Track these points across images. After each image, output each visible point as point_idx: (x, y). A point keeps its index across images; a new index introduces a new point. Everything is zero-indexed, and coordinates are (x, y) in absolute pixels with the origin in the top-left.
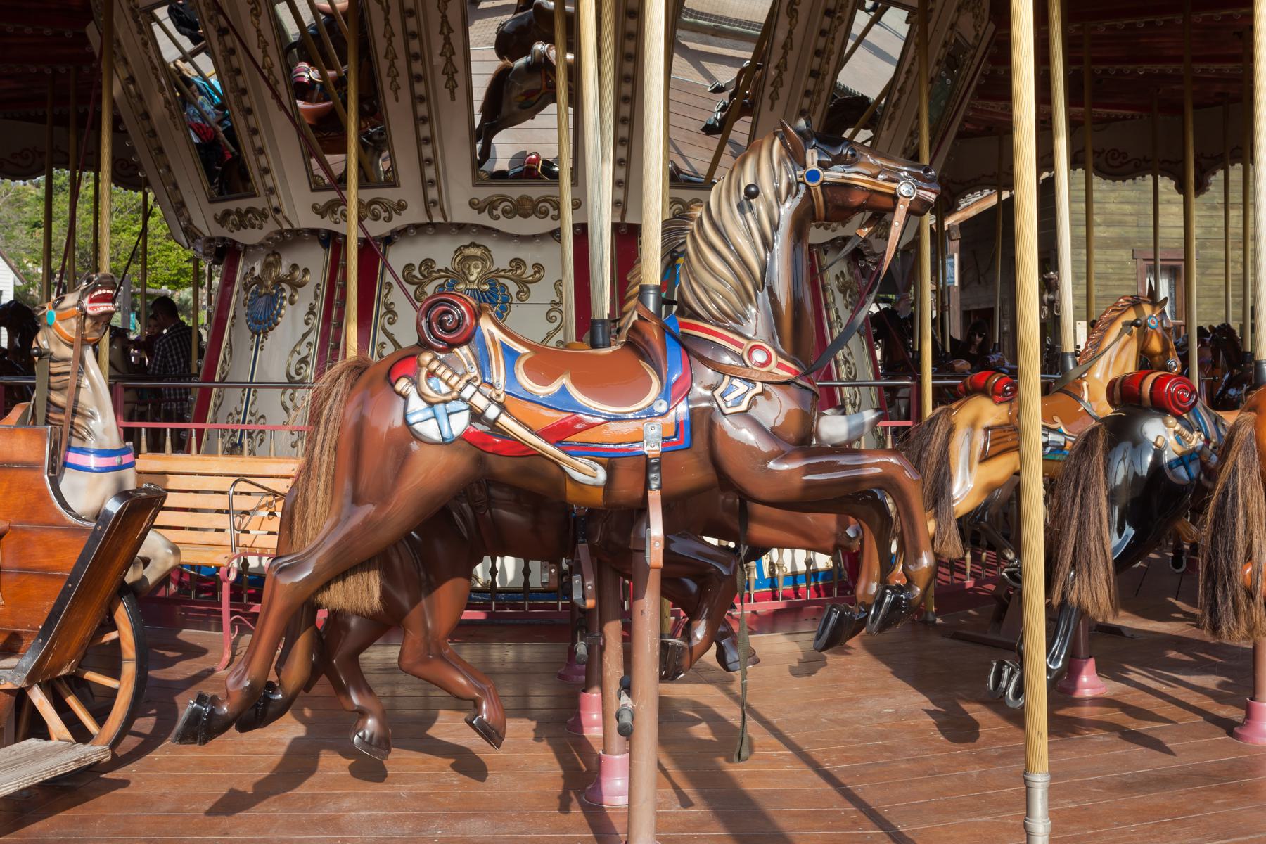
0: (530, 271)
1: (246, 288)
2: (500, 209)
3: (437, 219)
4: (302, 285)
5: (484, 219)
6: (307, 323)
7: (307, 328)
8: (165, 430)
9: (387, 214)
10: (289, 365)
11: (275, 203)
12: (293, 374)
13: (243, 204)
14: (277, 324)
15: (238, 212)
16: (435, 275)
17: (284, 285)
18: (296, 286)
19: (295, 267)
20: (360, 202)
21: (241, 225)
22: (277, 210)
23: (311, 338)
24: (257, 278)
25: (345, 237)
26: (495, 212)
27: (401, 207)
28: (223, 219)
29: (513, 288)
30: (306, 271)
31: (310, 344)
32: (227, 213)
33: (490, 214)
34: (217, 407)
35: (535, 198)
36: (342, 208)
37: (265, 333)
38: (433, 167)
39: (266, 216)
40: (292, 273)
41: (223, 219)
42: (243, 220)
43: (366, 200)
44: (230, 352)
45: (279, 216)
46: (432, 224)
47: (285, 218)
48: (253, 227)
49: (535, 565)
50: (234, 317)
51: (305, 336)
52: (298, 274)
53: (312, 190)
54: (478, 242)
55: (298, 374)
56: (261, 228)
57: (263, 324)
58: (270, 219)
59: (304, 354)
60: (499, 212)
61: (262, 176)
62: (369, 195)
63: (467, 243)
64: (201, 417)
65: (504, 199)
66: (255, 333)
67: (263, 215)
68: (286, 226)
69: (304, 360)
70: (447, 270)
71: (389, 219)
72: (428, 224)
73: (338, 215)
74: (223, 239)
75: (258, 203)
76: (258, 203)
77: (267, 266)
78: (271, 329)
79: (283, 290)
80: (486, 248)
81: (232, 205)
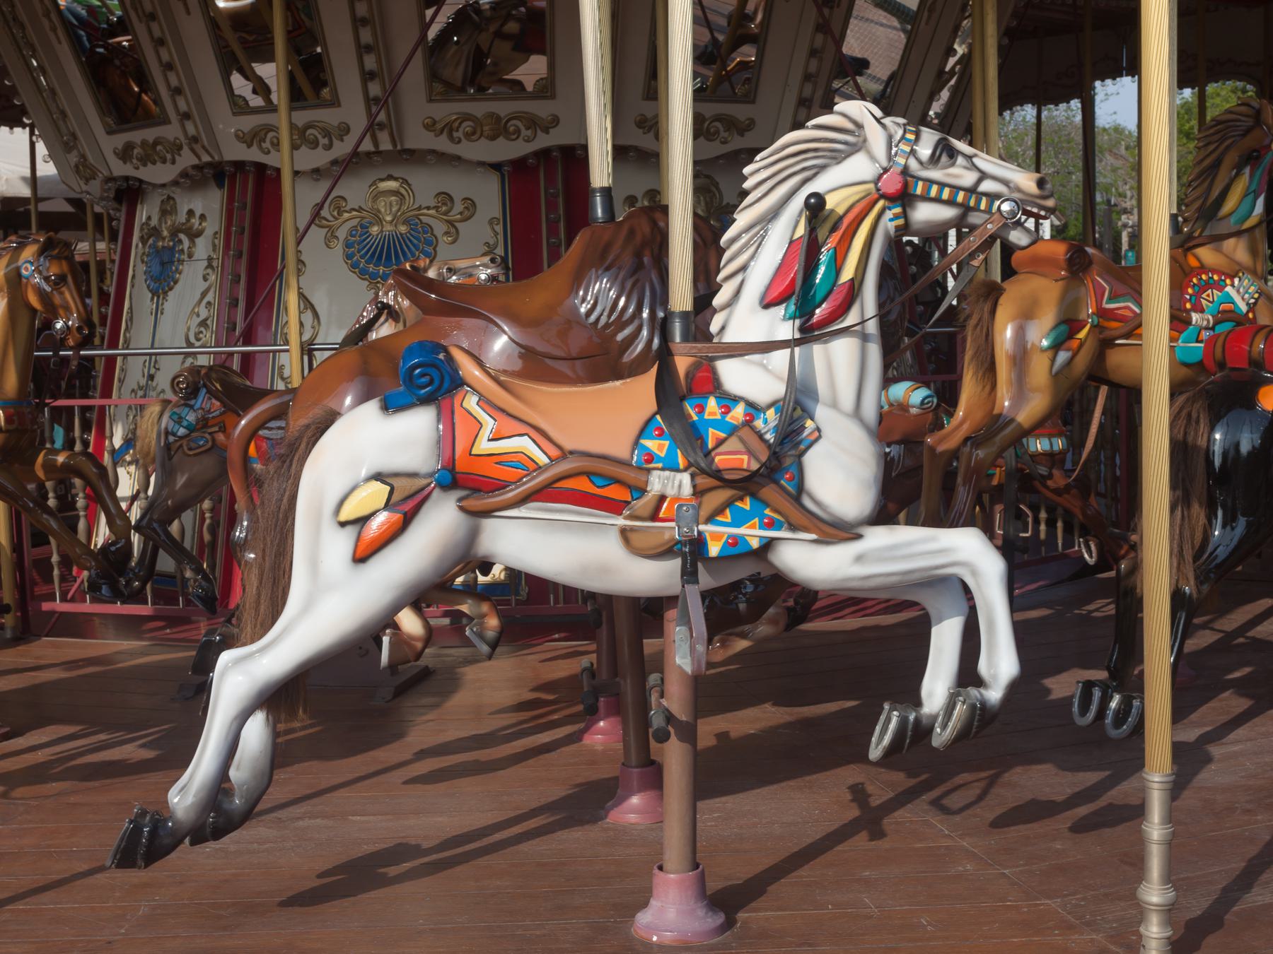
0: (459, 207)
1: (143, 240)
2: (268, 140)
3: (386, 145)
4: (199, 234)
5: (442, 144)
6: (205, 279)
7: (207, 284)
8: (72, 408)
9: (326, 141)
10: (189, 329)
11: (191, 130)
12: (192, 339)
13: (150, 134)
14: (176, 282)
15: (144, 143)
16: (346, 215)
17: (182, 236)
18: (194, 235)
19: (191, 213)
20: (292, 126)
21: (145, 160)
22: (195, 139)
23: (210, 297)
24: (154, 228)
25: (278, 171)
26: (455, 134)
27: (345, 130)
28: (125, 154)
29: (439, 228)
30: (203, 217)
31: (209, 303)
32: (129, 147)
33: (260, 148)
34: (121, 381)
35: (479, 116)
36: (271, 135)
37: (165, 293)
38: (377, 81)
39: (180, 148)
40: (188, 220)
41: (125, 154)
42: (150, 154)
43: (300, 124)
44: (131, 319)
45: (197, 147)
46: (378, 153)
47: (204, 147)
48: (164, 162)
49: (1054, 440)
50: (134, 276)
51: (204, 294)
52: (195, 221)
53: (234, 114)
54: (396, 175)
55: (198, 340)
56: (173, 162)
57: (162, 283)
58: (186, 151)
59: (203, 317)
60: (459, 134)
61: (173, 97)
62: (301, 117)
63: (384, 176)
64: (107, 393)
65: (466, 117)
66: (155, 293)
67: (177, 148)
68: (206, 158)
69: (203, 323)
70: (360, 209)
71: (329, 147)
72: (374, 153)
73: (267, 145)
74: (127, 179)
75: (171, 132)
76: (171, 132)
77: (164, 213)
78: (171, 289)
79: (180, 241)
80: (405, 181)
81: (137, 136)
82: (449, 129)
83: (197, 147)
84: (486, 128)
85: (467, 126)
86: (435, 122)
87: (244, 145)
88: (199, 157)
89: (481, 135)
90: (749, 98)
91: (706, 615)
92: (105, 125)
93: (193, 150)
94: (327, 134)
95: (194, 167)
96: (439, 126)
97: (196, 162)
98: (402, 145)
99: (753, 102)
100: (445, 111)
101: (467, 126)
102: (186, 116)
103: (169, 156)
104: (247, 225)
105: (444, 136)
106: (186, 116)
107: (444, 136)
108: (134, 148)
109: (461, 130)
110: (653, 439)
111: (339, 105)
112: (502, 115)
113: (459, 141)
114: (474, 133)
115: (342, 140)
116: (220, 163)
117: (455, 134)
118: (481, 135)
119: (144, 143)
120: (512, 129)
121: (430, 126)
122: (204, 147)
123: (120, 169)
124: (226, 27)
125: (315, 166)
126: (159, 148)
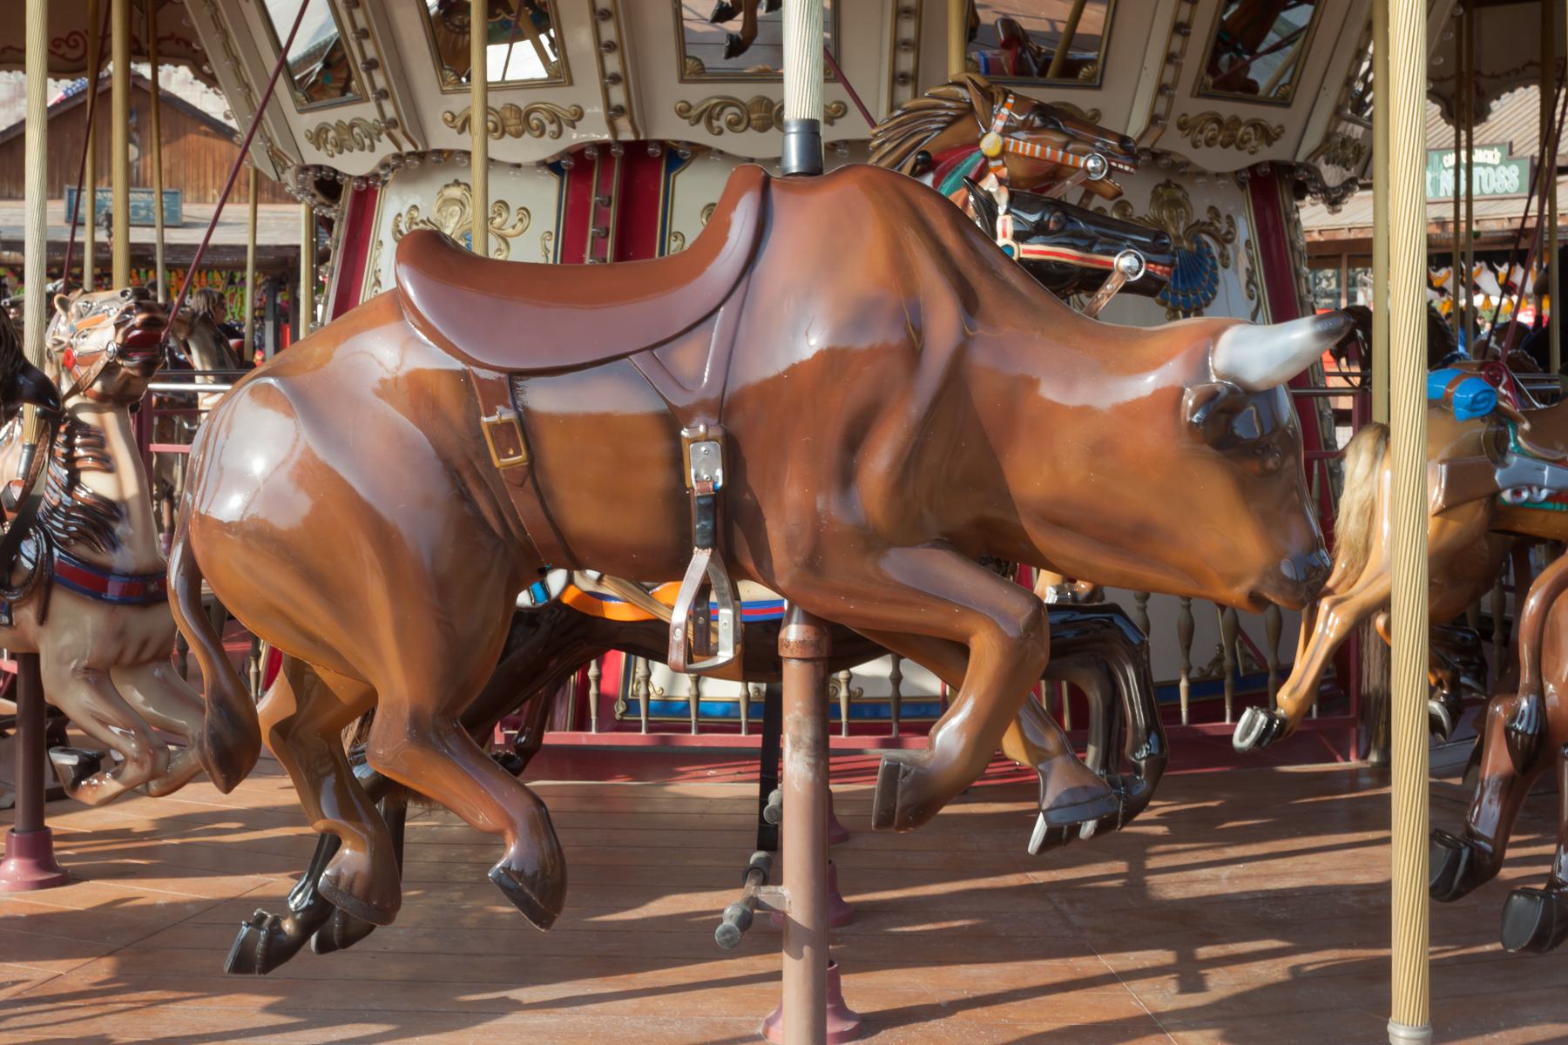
9: (554, 127)
21: (340, 147)
26: (715, 123)
28: (318, 137)
32: (323, 130)
45: (397, 133)
48: (362, 149)
56: (372, 149)
60: (722, 123)
63: (451, 181)
65: (729, 102)
68: (407, 148)
82: (708, 116)
83: (397, 133)
84: (753, 116)
85: (730, 113)
86: (690, 107)
87: (454, 131)
88: (398, 146)
89: (748, 124)
90: (1095, 84)
91: (16, 918)
92: (296, 101)
93: (391, 136)
94: (555, 118)
95: (396, 156)
96: (694, 113)
97: (396, 150)
98: (646, 133)
99: (1099, 87)
100: (700, 94)
101: (730, 113)
102: (383, 95)
103: (367, 142)
104: (612, 225)
105: (702, 126)
106: (383, 95)
107: (702, 126)
108: (327, 131)
109: (723, 118)
110: (1333, 560)
111: (571, 83)
112: (693, 102)
113: (721, 132)
114: (738, 122)
115: (574, 127)
116: (645, 143)
117: (715, 123)
118: (748, 124)
119: (340, 124)
120: (534, 123)
121: (684, 112)
122: (405, 133)
123: (314, 156)
125: (517, 161)
126: (356, 130)
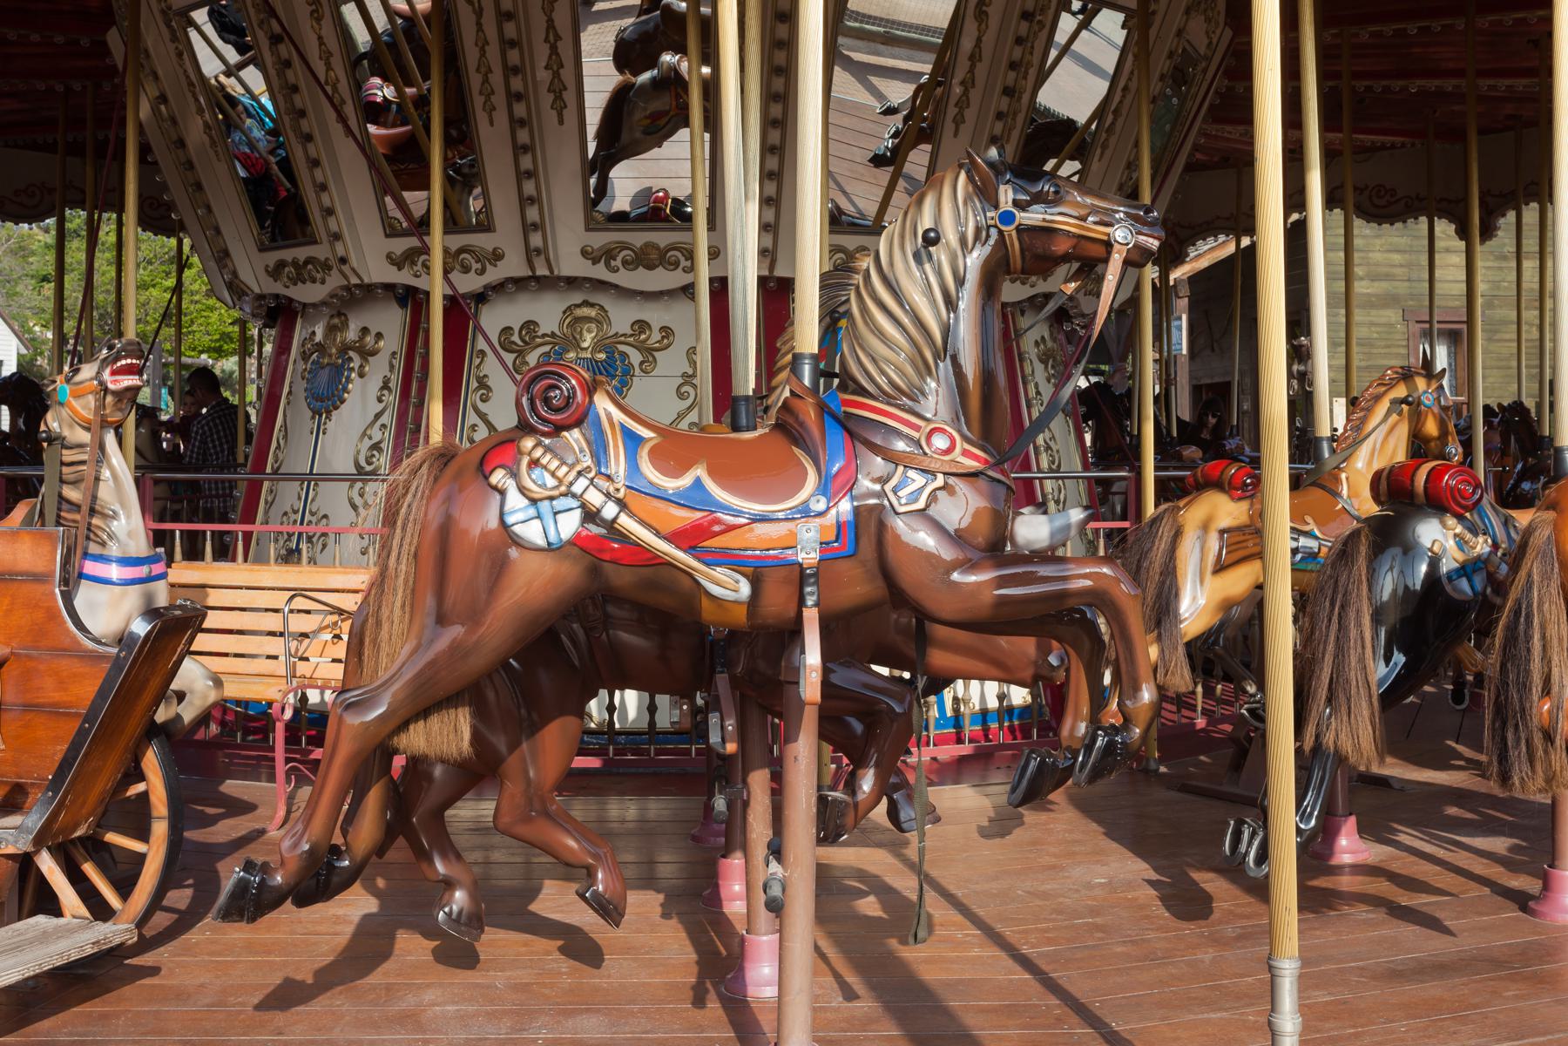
0: (656, 336)
1: (305, 356)
3: (542, 271)
4: (374, 353)
5: (600, 272)
6: (380, 400)
7: (380, 407)
8: (204, 532)
9: (479, 266)
10: (358, 452)
11: (340, 251)
12: (363, 463)
13: (302, 253)
14: (343, 401)
15: (295, 263)
16: (539, 340)
17: (351, 353)
18: (367, 354)
19: (365, 331)
20: (446, 251)
21: (299, 279)
22: (343, 261)
23: (385, 419)
24: (319, 344)
25: (427, 294)
26: (613, 263)
27: (497, 256)
28: (276, 272)
29: (635, 357)
30: (379, 336)
31: (384, 426)
32: (281, 264)
34: (269, 504)
35: (662, 246)
36: (423, 257)
37: (329, 413)
38: (536, 207)
39: (330, 268)
40: (361, 339)
41: (276, 272)
42: (301, 273)
43: (454, 248)
44: (285, 437)
45: (345, 268)
46: (535, 278)
47: (353, 270)
48: (314, 281)
49: (663, 700)
50: (290, 393)
51: (378, 416)
52: (369, 339)
53: (387, 236)
54: (592, 300)
55: (369, 464)
56: (323, 282)
57: (326, 401)
58: (334, 272)
59: (376, 439)
60: (618, 263)
61: (324, 219)
62: (457, 241)
63: (579, 301)
64: (249, 517)
65: (624, 246)
66: (316, 413)
67: (326, 267)
68: (354, 280)
69: (376, 447)
70: (553, 335)
71: (482, 272)
72: (530, 278)
73: (419, 267)
74: (277, 296)
75: (320, 252)
76: (320, 252)
77: (331, 330)
78: (336, 408)
79: (350, 359)
80: (602, 308)
81: (288, 255)
124: (87, 205)
